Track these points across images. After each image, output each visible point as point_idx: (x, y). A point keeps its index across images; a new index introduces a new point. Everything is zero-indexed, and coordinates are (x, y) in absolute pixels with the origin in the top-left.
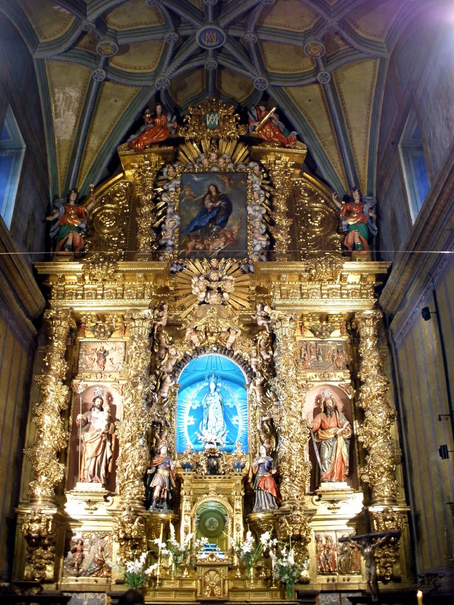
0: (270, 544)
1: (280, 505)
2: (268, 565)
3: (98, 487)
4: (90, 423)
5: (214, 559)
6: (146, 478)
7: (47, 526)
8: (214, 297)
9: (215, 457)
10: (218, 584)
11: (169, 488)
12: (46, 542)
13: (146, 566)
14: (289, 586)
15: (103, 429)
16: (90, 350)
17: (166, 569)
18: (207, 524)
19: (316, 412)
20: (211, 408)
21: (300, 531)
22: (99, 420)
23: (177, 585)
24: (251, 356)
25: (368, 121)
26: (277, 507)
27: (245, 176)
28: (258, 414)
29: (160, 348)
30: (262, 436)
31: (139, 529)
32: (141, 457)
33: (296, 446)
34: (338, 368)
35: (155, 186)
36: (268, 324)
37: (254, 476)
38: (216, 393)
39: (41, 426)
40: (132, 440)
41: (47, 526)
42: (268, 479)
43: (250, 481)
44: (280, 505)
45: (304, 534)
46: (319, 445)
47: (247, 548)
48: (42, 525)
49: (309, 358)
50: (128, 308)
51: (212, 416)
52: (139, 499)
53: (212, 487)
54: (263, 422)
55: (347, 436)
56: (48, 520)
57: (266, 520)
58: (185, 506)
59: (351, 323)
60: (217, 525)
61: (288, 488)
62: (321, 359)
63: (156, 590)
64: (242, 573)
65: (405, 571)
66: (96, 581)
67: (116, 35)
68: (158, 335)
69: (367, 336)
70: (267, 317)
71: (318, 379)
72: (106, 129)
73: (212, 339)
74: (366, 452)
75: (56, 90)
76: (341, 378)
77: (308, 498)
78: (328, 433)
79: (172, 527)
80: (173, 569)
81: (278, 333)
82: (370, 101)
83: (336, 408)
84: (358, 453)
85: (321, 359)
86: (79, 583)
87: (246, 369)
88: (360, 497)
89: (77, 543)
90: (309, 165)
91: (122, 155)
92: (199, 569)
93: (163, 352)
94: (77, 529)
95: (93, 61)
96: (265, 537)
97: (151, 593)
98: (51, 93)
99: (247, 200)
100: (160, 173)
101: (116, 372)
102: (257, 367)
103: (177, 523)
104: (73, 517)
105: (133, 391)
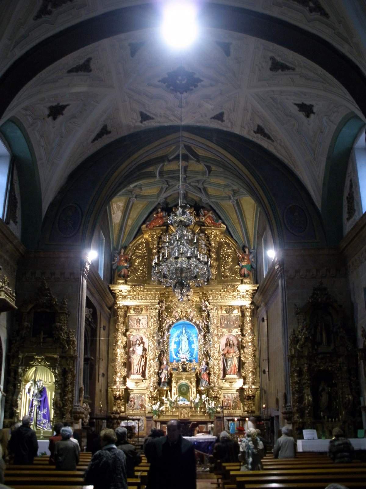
0: (206, 399)
1: (210, 384)
2: (205, 406)
3: (140, 377)
4: (135, 351)
5: (185, 405)
6: (159, 374)
7: (122, 393)
8: (184, 304)
9: (185, 364)
10: (186, 414)
11: (168, 377)
12: (122, 398)
13: (160, 407)
14: (212, 414)
15: (141, 354)
16: (133, 319)
17: (167, 408)
18: (182, 390)
19: (226, 345)
20: (183, 341)
21: (217, 394)
22: (139, 350)
23: (171, 414)
24: (199, 322)
25: (254, 216)
26: (208, 385)
28: (202, 347)
29: (162, 318)
30: (204, 356)
31: (157, 394)
32: (157, 366)
33: (216, 362)
34: (235, 328)
35: (158, 244)
36: (207, 310)
37: (200, 373)
38: (185, 335)
39: (117, 354)
40: (153, 359)
41: (122, 393)
42: (205, 375)
43: (198, 375)
45: (218, 396)
46: (226, 360)
47: (197, 401)
48: (120, 392)
49: (224, 323)
50: (149, 304)
51: (183, 345)
52: (156, 382)
53: (184, 377)
54: (204, 350)
55: (237, 356)
56: (122, 391)
57: (205, 390)
58: (174, 384)
59: (242, 310)
60: (186, 390)
61: (213, 378)
62: (229, 323)
63: (163, 416)
64: (195, 409)
65: (257, 409)
66: (140, 412)
67: (141, 186)
68: (162, 314)
69: (248, 316)
70: (206, 307)
71: (227, 332)
72: (135, 216)
73: (184, 314)
74: (244, 363)
75: (113, 204)
76: (236, 331)
77: (220, 381)
78: (230, 355)
79: (169, 393)
80: (170, 408)
81: (211, 314)
82: (254, 208)
83: (234, 344)
84: (241, 364)
85: (229, 323)
86: (134, 413)
87: (197, 327)
88: (242, 381)
89: (132, 398)
90: (228, 232)
91: (143, 230)
92: (179, 408)
93: (164, 320)
94: (132, 393)
95: (130, 194)
96: (204, 396)
97: (162, 417)
98: (111, 206)
101: (144, 329)
102: (202, 327)
103: (170, 390)
104: (130, 388)
105: (153, 340)
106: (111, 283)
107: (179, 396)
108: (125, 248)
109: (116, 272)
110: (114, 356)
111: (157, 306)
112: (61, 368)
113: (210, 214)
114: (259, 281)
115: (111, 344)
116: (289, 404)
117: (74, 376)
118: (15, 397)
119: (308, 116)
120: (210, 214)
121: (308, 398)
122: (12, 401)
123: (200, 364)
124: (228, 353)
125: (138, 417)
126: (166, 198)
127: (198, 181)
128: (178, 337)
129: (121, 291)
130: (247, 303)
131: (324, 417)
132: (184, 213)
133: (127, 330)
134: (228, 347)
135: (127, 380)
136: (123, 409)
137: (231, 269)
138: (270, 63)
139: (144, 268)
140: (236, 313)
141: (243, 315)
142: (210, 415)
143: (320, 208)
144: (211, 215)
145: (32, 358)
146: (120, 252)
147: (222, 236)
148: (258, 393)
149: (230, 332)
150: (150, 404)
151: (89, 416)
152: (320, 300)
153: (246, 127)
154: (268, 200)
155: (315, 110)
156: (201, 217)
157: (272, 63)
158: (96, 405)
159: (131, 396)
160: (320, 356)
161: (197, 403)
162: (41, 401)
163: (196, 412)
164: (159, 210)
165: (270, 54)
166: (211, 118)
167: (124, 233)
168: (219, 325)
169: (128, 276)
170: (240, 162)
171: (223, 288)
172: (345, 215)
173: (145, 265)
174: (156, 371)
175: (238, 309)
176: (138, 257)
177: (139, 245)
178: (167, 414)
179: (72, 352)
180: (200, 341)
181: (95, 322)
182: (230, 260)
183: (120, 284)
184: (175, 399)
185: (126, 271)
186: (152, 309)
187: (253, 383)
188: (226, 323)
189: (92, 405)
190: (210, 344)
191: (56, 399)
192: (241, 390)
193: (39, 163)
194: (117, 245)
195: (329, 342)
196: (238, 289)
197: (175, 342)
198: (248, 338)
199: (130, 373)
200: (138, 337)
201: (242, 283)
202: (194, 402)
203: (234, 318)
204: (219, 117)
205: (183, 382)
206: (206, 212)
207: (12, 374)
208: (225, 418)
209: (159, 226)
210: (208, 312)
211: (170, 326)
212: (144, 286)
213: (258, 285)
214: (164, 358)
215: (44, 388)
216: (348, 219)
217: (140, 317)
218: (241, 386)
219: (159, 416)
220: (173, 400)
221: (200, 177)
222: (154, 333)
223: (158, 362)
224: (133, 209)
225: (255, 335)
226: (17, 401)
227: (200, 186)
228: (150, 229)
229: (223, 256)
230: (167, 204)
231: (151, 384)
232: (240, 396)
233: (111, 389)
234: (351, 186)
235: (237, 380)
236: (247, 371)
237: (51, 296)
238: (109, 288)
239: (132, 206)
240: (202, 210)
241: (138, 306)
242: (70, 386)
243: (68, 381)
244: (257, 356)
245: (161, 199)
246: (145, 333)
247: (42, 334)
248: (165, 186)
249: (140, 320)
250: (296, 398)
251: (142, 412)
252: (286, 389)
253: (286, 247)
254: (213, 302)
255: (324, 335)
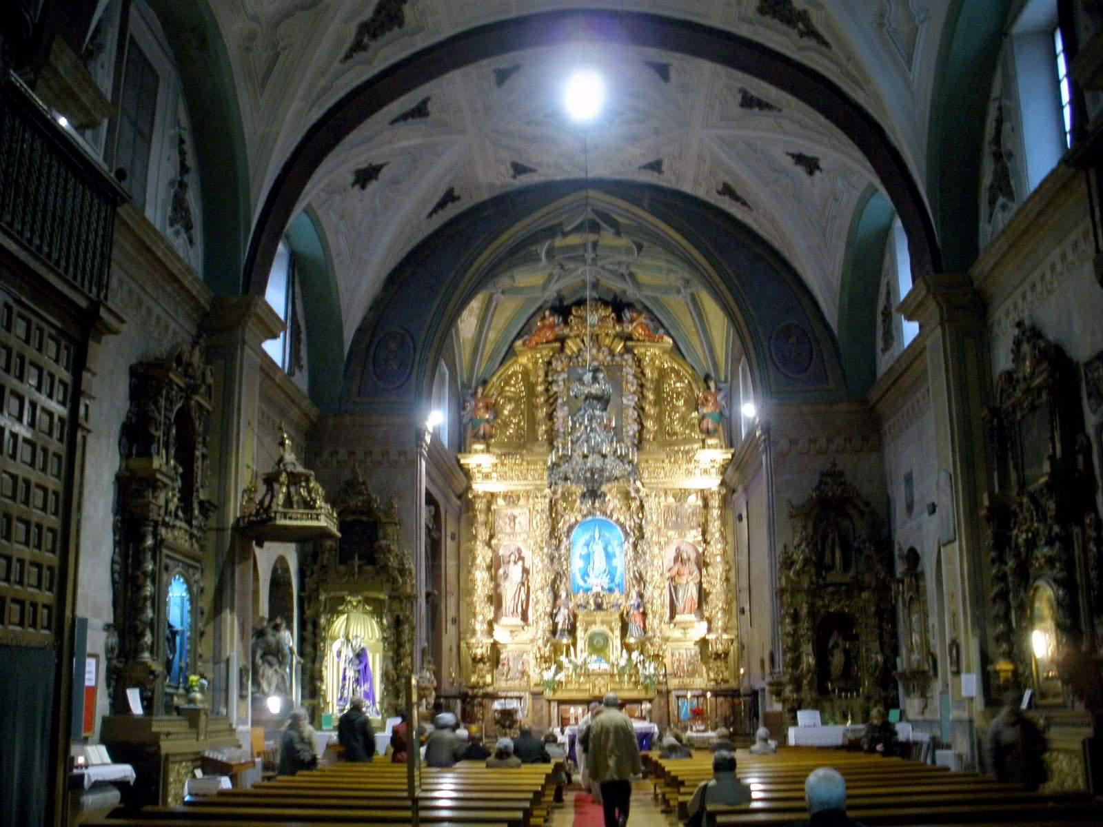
1: (645, 632)
2: (638, 672)
3: (518, 621)
6: (552, 616)
13: (556, 673)
18: (595, 642)
19: (676, 560)
22: (515, 572)
27: (621, 367)
33: (656, 594)
34: (692, 528)
35: (546, 375)
37: (628, 613)
40: (542, 589)
44: (645, 632)
46: (675, 588)
47: (623, 662)
48: (484, 650)
57: (636, 643)
58: (580, 633)
68: (555, 504)
70: (638, 491)
76: (694, 535)
77: (664, 626)
83: (689, 559)
84: (703, 596)
88: (704, 624)
90: (676, 349)
96: (635, 655)
99: (622, 390)
100: (549, 363)
103: (574, 644)
106: (460, 451)
107: (590, 654)
108: (485, 383)
109: (470, 426)
110: (470, 585)
111: (547, 491)
112: (392, 616)
113: (642, 319)
114: (735, 442)
115: (465, 563)
116: (777, 670)
117: (413, 629)
118: (317, 665)
119: (811, 173)
120: (642, 319)
121: (809, 660)
122: (313, 670)
123: (628, 596)
124: (679, 574)
125: (516, 694)
126: (559, 292)
127: (620, 263)
128: (587, 545)
129: (479, 465)
130: (712, 482)
131: (834, 691)
132: (595, 379)
133: (492, 537)
134: (679, 564)
135: (496, 626)
136: (488, 679)
137: (683, 419)
138: (739, 97)
139: (519, 421)
140: (694, 501)
141: (706, 505)
142: (646, 688)
143: (836, 332)
144: (644, 321)
145: (342, 600)
146: (475, 393)
147: (666, 357)
148: (733, 649)
149: (682, 535)
150: (538, 670)
151: (434, 693)
152: (830, 494)
153: (704, 184)
154: (743, 316)
155: (822, 164)
156: (625, 325)
157: (743, 98)
158: (444, 674)
159: (502, 657)
160: (830, 589)
161: (623, 668)
162: (359, 671)
163: (621, 682)
164: (547, 313)
165: (739, 85)
166: (640, 168)
167: (482, 356)
168: (662, 524)
169: (491, 437)
170: (693, 244)
171: (668, 456)
172: (880, 344)
173: (522, 413)
174: (548, 610)
175: (697, 493)
176: (510, 400)
177: (510, 377)
178: (569, 686)
179: (409, 590)
180: (626, 555)
181: (439, 529)
182: (681, 403)
183: (476, 452)
184: (582, 659)
185: (487, 427)
186: (537, 497)
187: (725, 630)
188: (674, 519)
189: (437, 674)
190: (645, 560)
191: (387, 667)
192: (704, 643)
193: (335, 261)
194: (470, 379)
195: (846, 566)
196: (696, 458)
197: (581, 556)
198: (716, 548)
199: (499, 614)
200: (513, 548)
201: (704, 447)
202: (617, 665)
203: (690, 510)
204: (656, 166)
205: (595, 628)
206: (635, 315)
207: (310, 627)
208: (674, 694)
209: (548, 342)
210: (641, 502)
211: (571, 528)
212: (521, 455)
213: (732, 451)
214: (562, 587)
215: (363, 650)
216: (884, 350)
217: (516, 511)
218: (703, 636)
219: (555, 691)
220: (579, 661)
221: (623, 258)
222: (542, 541)
223: (551, 594)
224: (497, 313)
225: (727, 543)
226: (321, 672)
227: (623, 270)
228: (531, 348)
229: (668, 395)
230: (561, 299)
231: (540, 634)
232: (701, 653)
233: (467, 643)
234: (888, 294)
235: (696, 624)
236: (715, 608)
237: (369, 495)
238: (458, 461)
239: (495, 308)
240: (626, 311)
241: (512, 492)
242: (408, 646)
243: (405, 637)
244: (733, 580)
245: (551, 294)
246: (525, 541)
247: (356, 558)
248: (557, 271)
249: (515, 517)
250: (787, 660)
251: (524, 683)
252: (773, 644)
253: (773, 401)
254: (650, 483)
255: (838, 555)
